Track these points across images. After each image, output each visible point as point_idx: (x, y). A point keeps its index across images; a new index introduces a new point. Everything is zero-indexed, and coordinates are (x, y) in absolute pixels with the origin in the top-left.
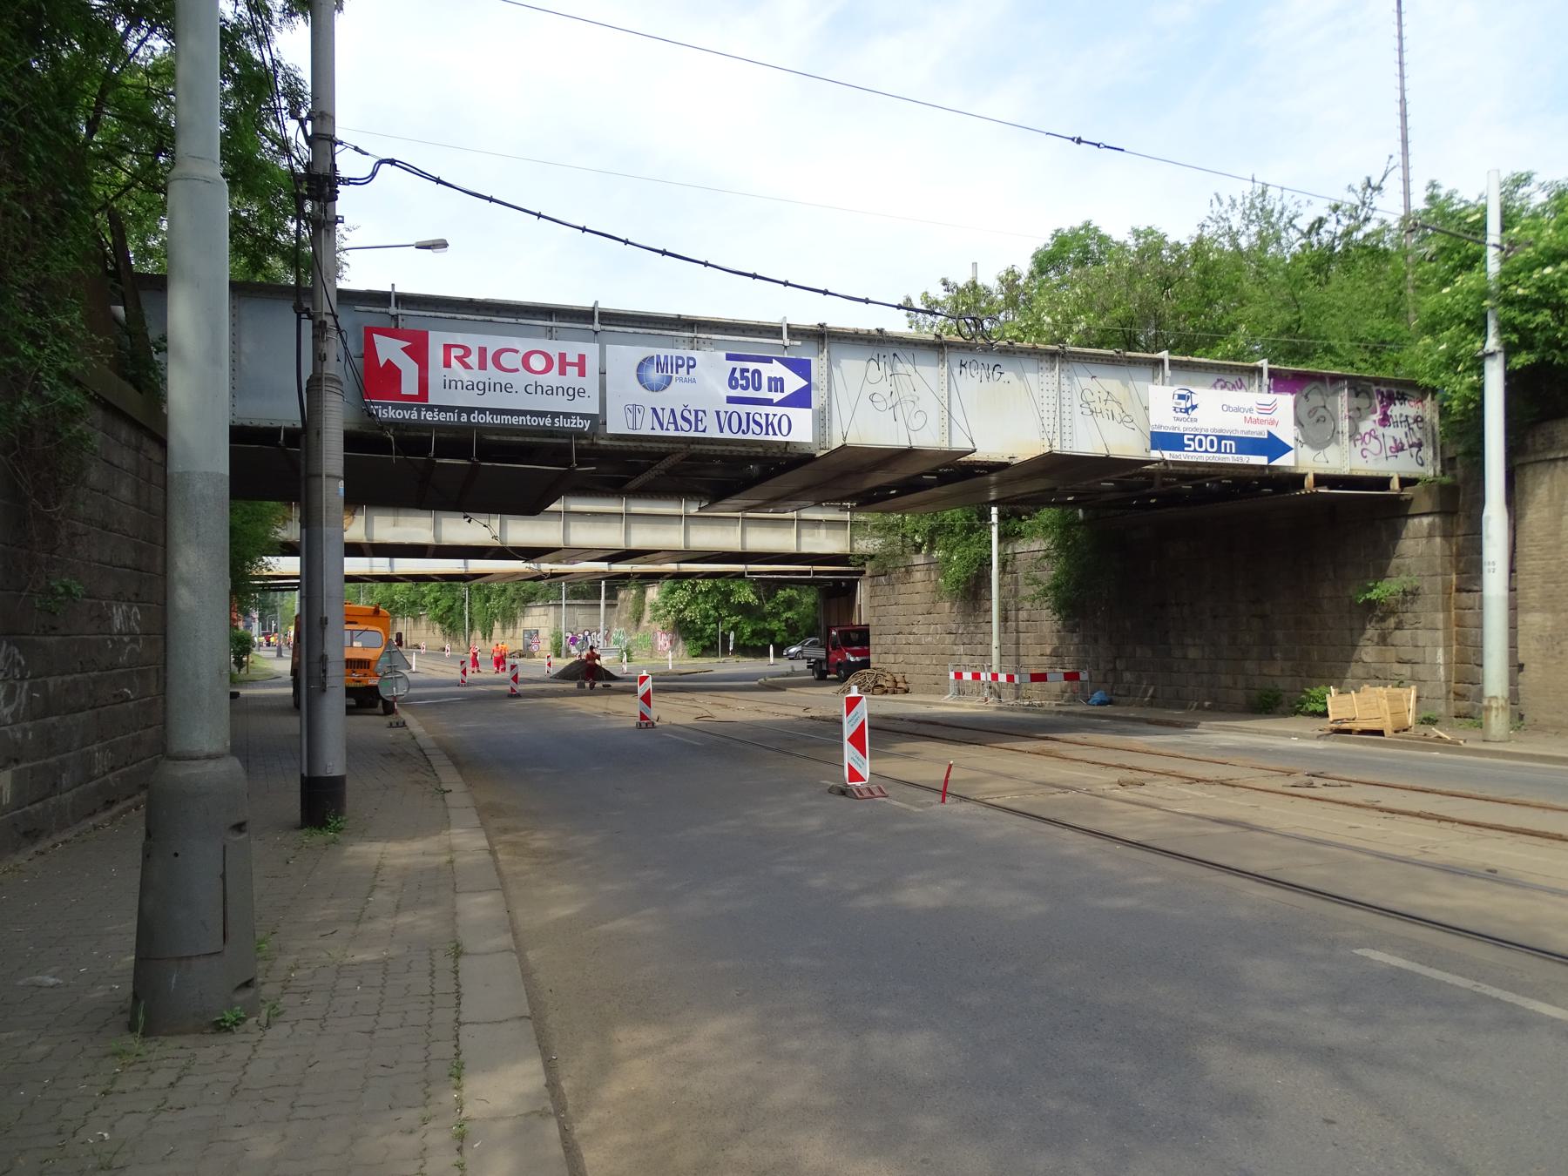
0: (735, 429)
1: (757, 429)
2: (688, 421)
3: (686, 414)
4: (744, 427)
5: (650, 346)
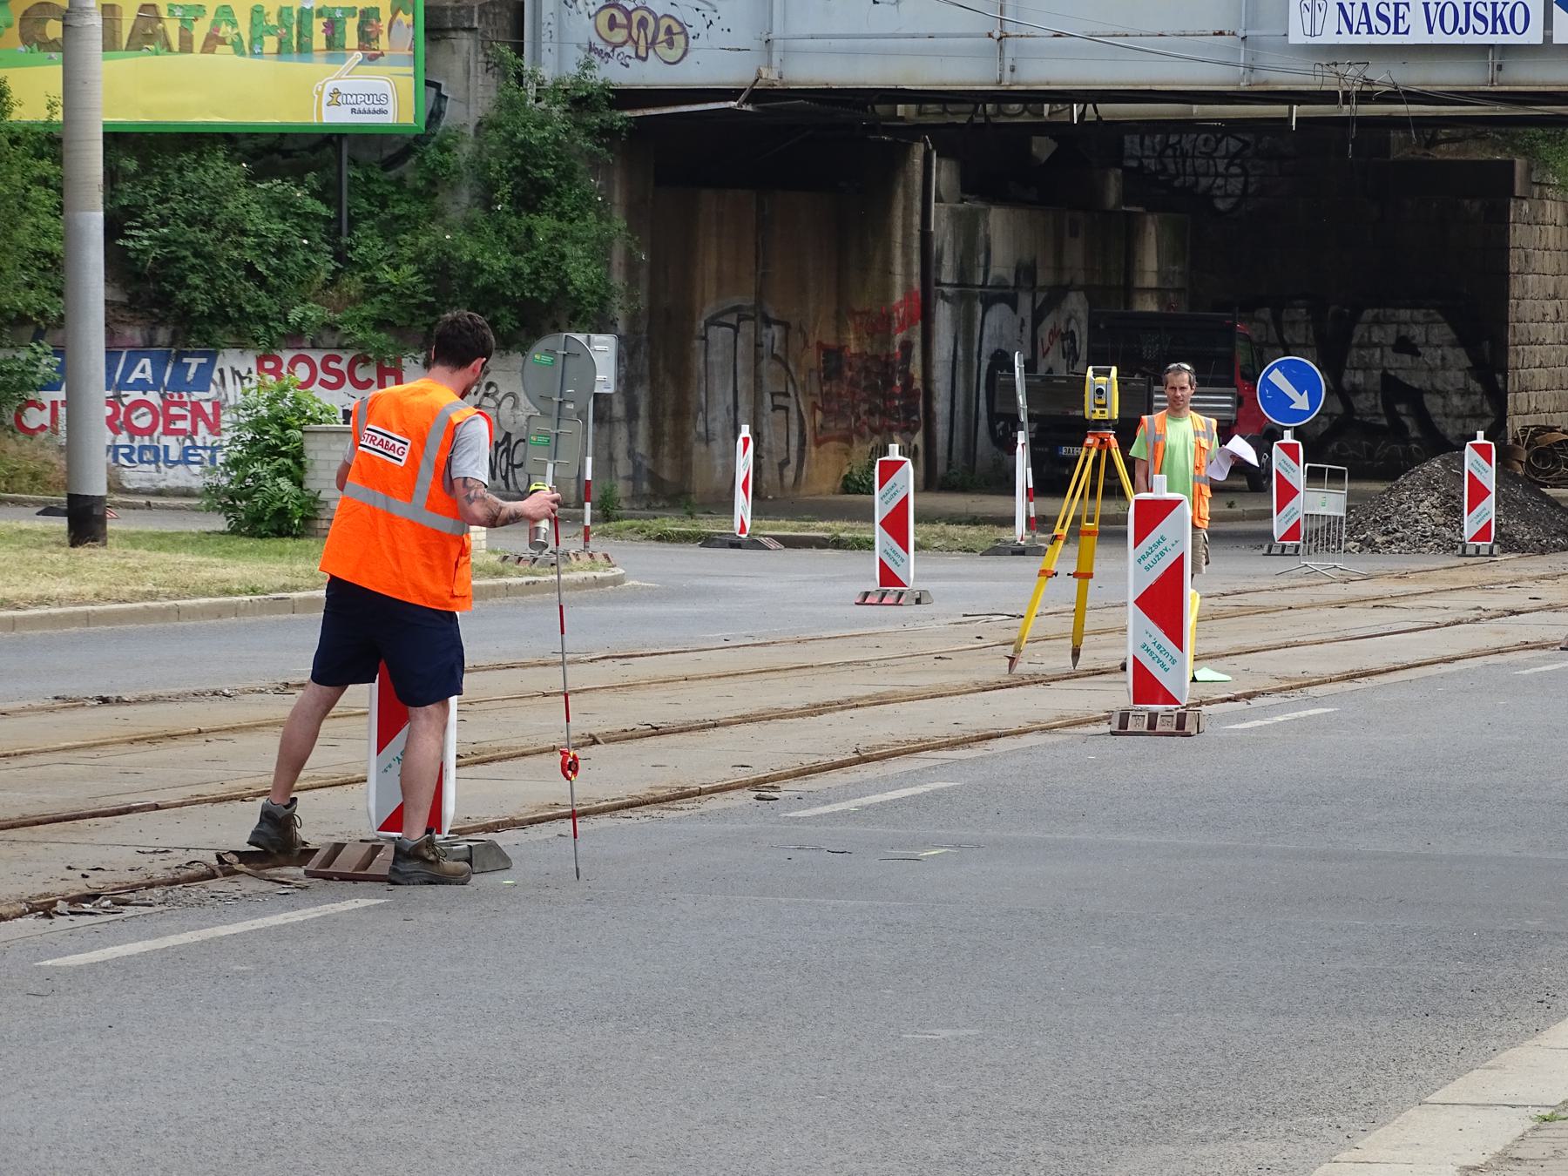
0: (1449, 28)
1: (1480, 26)
2: (1478, 16)
3: (1383, 9)
4: (1462, 24)
5: (378, 126)
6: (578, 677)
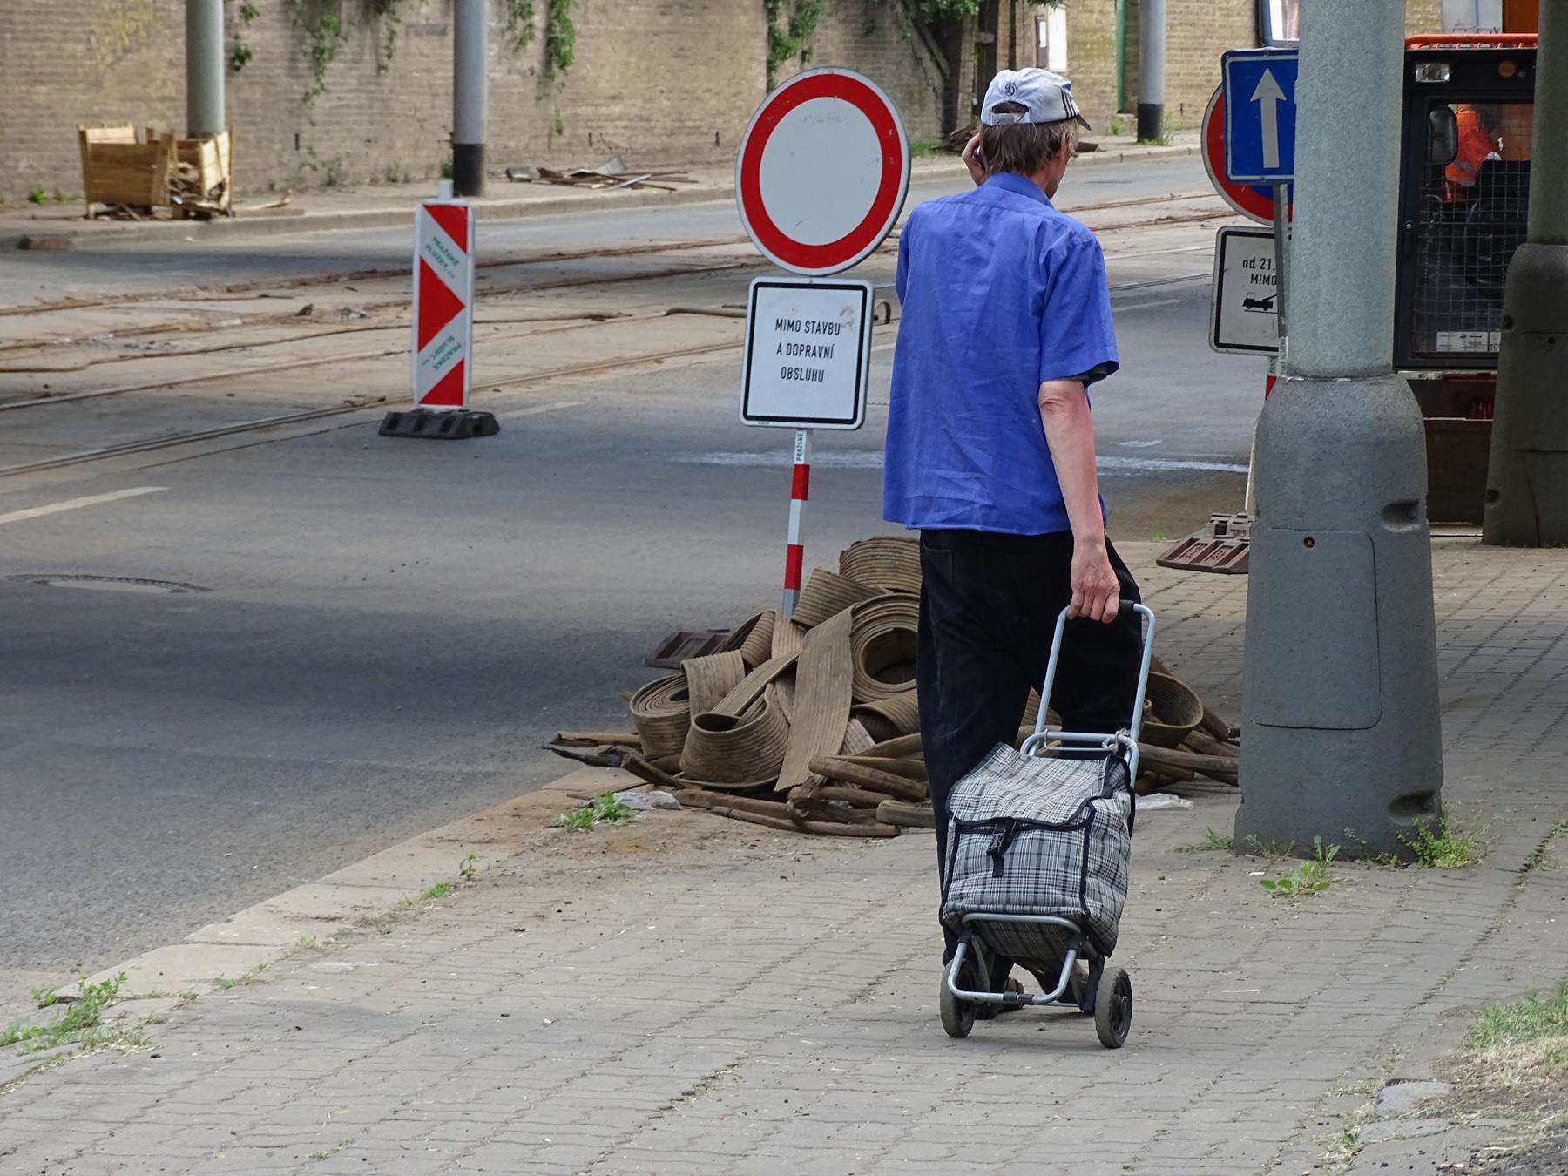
6: (508, 353)
